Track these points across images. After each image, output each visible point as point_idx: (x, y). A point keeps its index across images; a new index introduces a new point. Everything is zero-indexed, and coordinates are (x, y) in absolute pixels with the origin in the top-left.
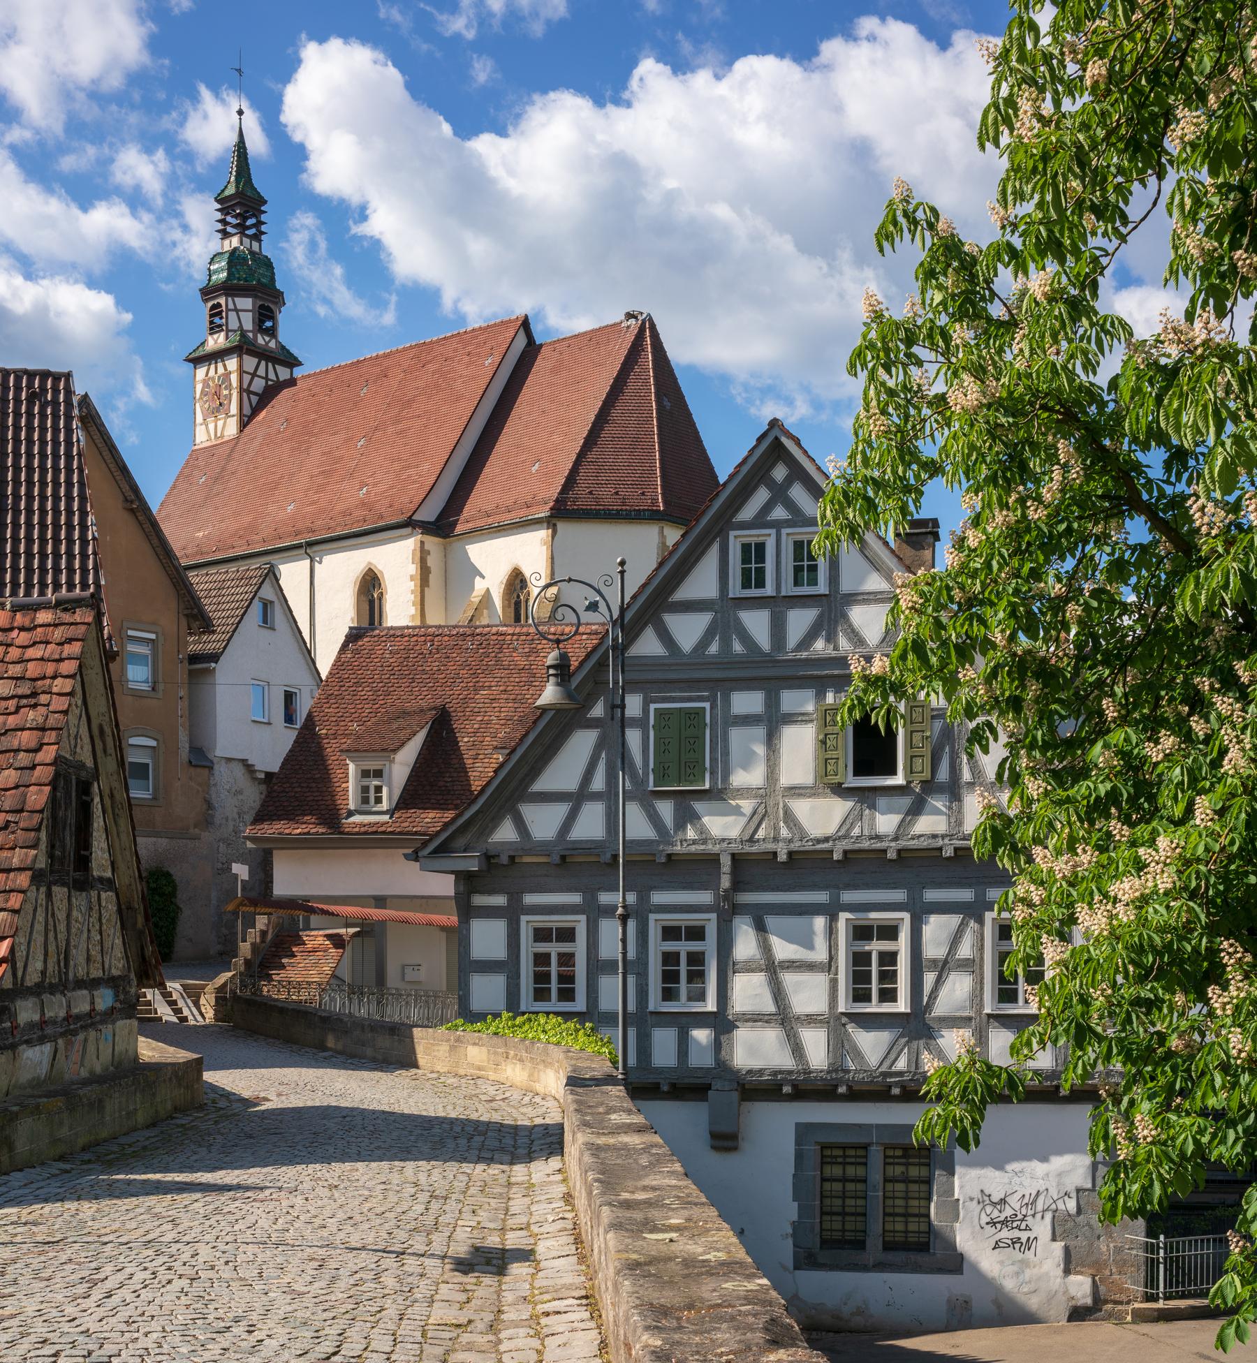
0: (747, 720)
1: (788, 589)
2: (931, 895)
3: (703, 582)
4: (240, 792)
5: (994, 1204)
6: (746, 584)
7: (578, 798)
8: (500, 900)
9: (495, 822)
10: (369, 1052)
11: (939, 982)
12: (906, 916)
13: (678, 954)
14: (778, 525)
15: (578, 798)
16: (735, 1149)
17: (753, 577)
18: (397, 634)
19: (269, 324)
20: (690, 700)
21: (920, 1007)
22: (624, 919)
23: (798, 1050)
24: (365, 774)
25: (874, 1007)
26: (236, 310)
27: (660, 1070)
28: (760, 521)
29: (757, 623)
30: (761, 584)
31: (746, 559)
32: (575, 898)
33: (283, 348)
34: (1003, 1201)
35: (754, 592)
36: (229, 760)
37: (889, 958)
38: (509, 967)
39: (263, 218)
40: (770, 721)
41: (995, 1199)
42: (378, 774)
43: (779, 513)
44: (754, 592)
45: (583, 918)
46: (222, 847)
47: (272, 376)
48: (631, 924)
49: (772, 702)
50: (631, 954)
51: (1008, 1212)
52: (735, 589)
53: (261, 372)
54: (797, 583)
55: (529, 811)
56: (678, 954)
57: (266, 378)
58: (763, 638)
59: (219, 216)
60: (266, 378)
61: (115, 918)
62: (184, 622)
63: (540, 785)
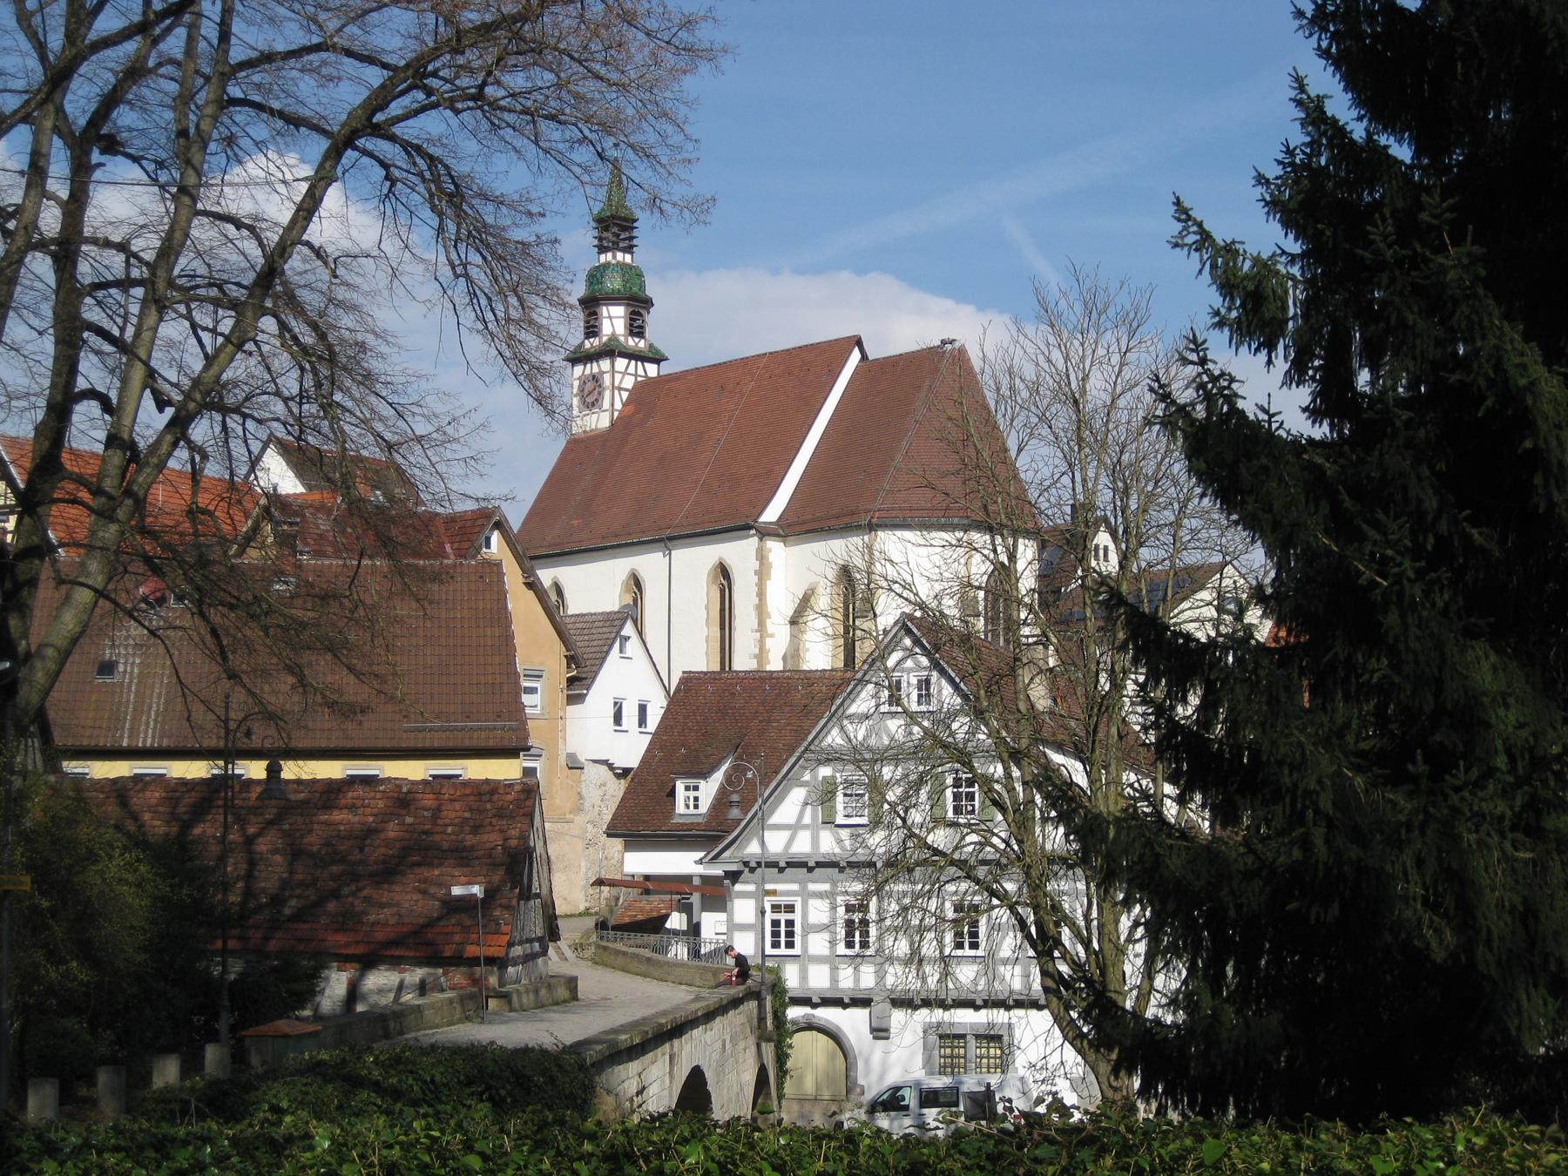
7: (795, 828)
8: (751, 888)
9: (748, 841)
10: (672, 978)
15: (795, 828)
21: (992, 954)
24: (687, 788)
26: (610, 318)
27: (842, 990)
32: (795, 887)
33: (651, 346)
36: (319, 253)
37: (790, 923)
39: (635, 233)
42: (696, 788)
47: (641, 372)
53: (631, 370)
54: (919, 703)
57: (636, 375)
60: (636, 375)
61: (991, 1025)
63: (773, 820)
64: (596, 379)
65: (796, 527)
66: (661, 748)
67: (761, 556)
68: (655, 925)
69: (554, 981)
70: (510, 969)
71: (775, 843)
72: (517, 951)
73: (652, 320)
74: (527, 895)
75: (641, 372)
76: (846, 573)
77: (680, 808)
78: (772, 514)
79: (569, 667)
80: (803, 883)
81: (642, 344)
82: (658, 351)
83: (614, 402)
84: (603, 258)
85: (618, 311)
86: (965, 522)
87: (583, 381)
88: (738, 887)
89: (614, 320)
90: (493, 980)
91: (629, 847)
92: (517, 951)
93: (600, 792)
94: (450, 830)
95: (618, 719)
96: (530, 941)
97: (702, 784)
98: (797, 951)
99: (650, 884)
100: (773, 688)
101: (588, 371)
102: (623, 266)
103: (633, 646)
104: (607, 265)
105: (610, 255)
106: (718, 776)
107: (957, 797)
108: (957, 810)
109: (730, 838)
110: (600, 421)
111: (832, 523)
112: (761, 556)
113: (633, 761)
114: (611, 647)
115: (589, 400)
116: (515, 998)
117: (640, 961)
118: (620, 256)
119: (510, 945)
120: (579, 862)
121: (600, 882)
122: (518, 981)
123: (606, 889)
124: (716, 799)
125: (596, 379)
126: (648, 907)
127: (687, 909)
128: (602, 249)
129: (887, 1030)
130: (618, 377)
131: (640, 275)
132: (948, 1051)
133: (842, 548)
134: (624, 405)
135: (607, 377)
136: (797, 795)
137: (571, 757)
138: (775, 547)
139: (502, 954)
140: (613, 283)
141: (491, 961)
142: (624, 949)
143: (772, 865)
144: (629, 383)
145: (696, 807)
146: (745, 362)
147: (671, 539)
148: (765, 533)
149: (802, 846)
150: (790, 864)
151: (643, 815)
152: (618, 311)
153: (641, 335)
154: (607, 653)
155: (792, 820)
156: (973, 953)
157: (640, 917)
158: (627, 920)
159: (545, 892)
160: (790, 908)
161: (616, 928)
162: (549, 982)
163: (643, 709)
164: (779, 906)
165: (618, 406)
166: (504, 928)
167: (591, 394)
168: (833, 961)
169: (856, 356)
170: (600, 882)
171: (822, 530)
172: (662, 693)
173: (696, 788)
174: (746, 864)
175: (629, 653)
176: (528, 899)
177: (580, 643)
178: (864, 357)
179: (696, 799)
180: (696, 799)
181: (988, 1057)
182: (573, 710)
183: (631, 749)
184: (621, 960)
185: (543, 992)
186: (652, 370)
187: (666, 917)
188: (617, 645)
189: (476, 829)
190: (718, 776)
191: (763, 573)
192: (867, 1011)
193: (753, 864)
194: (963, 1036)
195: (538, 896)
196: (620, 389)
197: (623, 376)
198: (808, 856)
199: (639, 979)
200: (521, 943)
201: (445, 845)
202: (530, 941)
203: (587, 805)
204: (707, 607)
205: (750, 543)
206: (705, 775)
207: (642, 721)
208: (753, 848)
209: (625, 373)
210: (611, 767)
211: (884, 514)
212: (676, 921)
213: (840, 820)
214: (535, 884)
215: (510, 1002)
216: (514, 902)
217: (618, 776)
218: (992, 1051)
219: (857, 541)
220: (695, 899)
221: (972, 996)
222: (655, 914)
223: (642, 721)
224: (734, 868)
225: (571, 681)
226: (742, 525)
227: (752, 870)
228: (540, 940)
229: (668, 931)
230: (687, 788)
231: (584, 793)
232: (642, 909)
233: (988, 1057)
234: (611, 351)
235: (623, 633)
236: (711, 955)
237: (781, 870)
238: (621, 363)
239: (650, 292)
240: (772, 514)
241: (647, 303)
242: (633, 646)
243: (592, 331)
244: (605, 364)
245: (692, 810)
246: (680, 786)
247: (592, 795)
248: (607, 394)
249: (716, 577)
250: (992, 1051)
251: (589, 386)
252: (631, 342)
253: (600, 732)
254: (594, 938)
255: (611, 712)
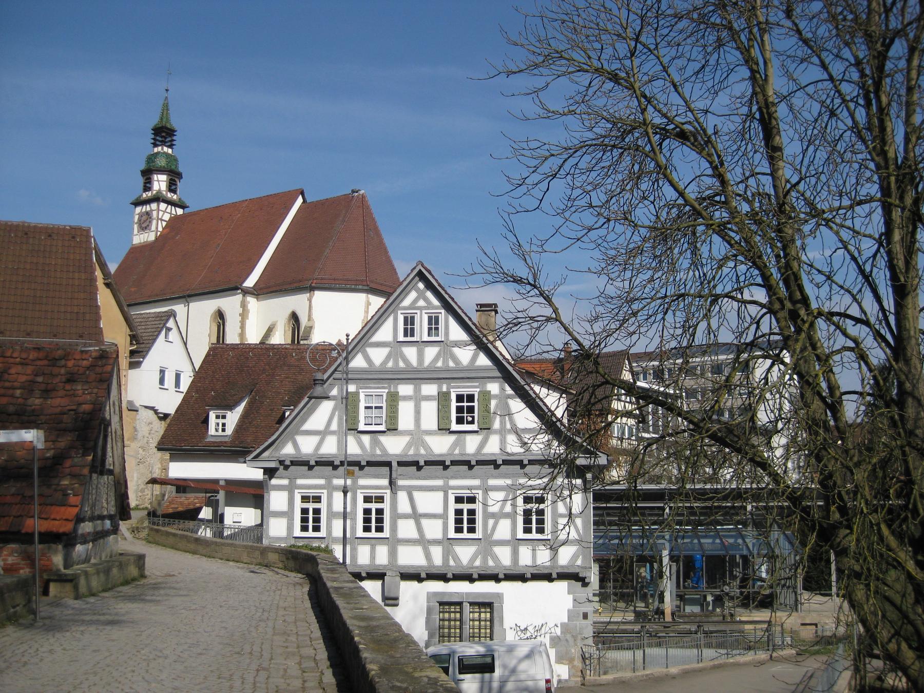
0: (406, 398)
1: (426, 338)
2: (492, 482)
3: (385, 333)
4: (151, 423)
5: (522, 631)
6: (406, 335)
7: (323, 434)
8: (285, 482)
9: (284, 445)
11: (496, 524)
12: (325, 491)
13: (468, 532)
14: (420, 308)
15: (323, 434)
16: (397, 605)
17: (409, 331)
18: (234, 347)
19: (173, 187)
20: (378, 388)
22: (345, 493)
23: (428, 556)
24: (217, 417)
25: (465, 535)
26: (158, 181)
27: (361, 566)
28: (413, 306)
29: (411, 353)
30: (412, 335)
31: (406, 323)
32: (322, 482)
34: (526, 629)
35: (409, 339)
38: (289, 514)
39: (174, 138)
40: (416, 399)
41: (522, 628)
42: (224, 417)
43: (421, 303)
44: (409, 339)
45: (325, 491)
46: (141, 451)
47: (173, 212)
48: (349, 495)
49: (417, 390)
50: (348, 510)
51: (528, 634)
52: (401, 338)
53: (169, 210)
55: (300, 439)
56: (468, 532)
57: (171, 213)
58: (414, 361)
59: (153, 136)
60: (171, 213)
62: (129, 338)
64: (148, 214)
65: (264, 290)
66: (197, 392)
67: (244, 305)
68: (192, 514)
69: (123, 559)
70: (79, 548)
71: (307, 446)
72: (87, 527)
73: (180, 185)
74: (99, 467)
75: (173, 212)
76: (294, 317)
77: (212, 431)
78: (250, 282)
79: (131, 344)
80: (329, 479)
81: (175, 197)
82: (183, 202)
83: (157, 228)
84: (156, 150)
85: (163, 177)
86: (366, 288)
87: (141, 215)
88: (274, 482)
89: (160, 182)
90: (58, 560)
91: (173, 458)
92: (87, 527)
93: (148, 428)
94: (18, 392)
95: (162, 381)
96: (102, 518)
97: (229, 414)
98: (386, 533)
99: (182, 486)
100: (274, 354)
101: (144, 210)
102: (166, 154)
103: (174, 335)
104: (158, 153)
105: (160, 148)
106: (240, 409)
107: (459, 410)
108: (460, 421)
109: (270, 441)
110: (151, 237)
111: (288, 287)
112: (244, 305)
113: (171, 410)
114: (160, 332)
115: (144, 226)
116: (82, 582)
117: (189, 541)
118: (165, 149)
119: (79, 519)
120: (142, 462)
121: (153, 481)
122: (87, 560)
123: (157, 487)
124: (237, 425)
125: (148, 214)
126: (186, 502)
127: (214, 504)
128: (155, 145)
129: (397, 599)
130: (161, 213)
131: (176, 160)
132: (447, 615)
133: (296, 302)
134: (163, 229)
135: (155, 213)
136: (326, 407)
137: (130, 403)
138: (251, 301)
139: (68, 527)
140: (161, 162)
141: (51, 538)
142: (173, 531)
143: (305, 463)
144: (167, 217)
145: (223, 430)
146: (234, 205)
147: (189, 296)
148: (246, 292)
149: (330, 447)
150: (318, 463)
151: (184, 434)
152: (163, 177)
153: (174, 191)
154: (157, 336)
155: (321, 427)
156: (539, 536)
157: (181, 509)
158: (171, 511)
159: (117, 470)
160: (317, 499)
161: (165, 516)
162: (121, 561)
163: (178, 376)
164: (308, 497)
165: (160, 229)
166: (72, 500)
167: (145, 223)
168: (515, 543)
169: (300, 200)
170: (153, 481)
171: (281, 291)
172: (191, 368)
173: (224, 417)
174: (281, 462)
175: (171, 338)
176: (102, 473)
177: (140, 330)
178: (304, 201)
179: (224, 425)
180: (224, 425)
181: (480, 620)
182: (133, 373)
183: (170, 402)
184: (171, 540)
185: (115, 571)
186: (180, 211)
187: (199, 510)
188: (163, 332)
189: (47, 392)
190: (240, 409)
191: (244, 315)
192: (379, 583)
193: (288, 463)
194: (460, 604)
195: (111, 472)
196: (162, 220)
197: (164, 213)
198: (334, 456)
199: (189, 556)
200: (92, 519)
201: (11, 409)
202: (102, 518)
203: (140, 435)
204: (209, 336)
205: (238, 298)
206: (231, 407)
207: (177, 384)
208: (288, 450)
209: (165, 212)
210: (156, 412)
211: (319, 281)
212: (206, 513)
213: (362, 427)
214: (109, 460)
215: (76, 588)
216: (86, 471)
217: (161, 419)
218: (483, 615)
219: (303, 298)
220: (221, 496)
221: (470, 571)
222: (192, 507)
223: (177, 384)
224: (272, 465)
225: (132, 353)
226: (233, 288)
227: (286, 468)
228: (111, 517)
229: (202, 520)
230: (217, 417)
231: (138, 427)
232: (182, 503)
233: (480, 620)
234: (157, 199)
235: (168, 325)
236: (230, 537)
237: (311, 468)
238: (163, 206)
239: (181, 170)
240: (250, 282)
241: (179, 175)
242: (174, 335)
243: (147, 187)
244: (154, 206)
245: (220, 433)
246: (212, 415)
247: (143, 430)
248: (154, 222)
249: (215, 318)
250: (483, 615)
251: (144, 218)
252: (169, 195)
253: (154, 384)
254: (146, 524)
255: (157, 377)
